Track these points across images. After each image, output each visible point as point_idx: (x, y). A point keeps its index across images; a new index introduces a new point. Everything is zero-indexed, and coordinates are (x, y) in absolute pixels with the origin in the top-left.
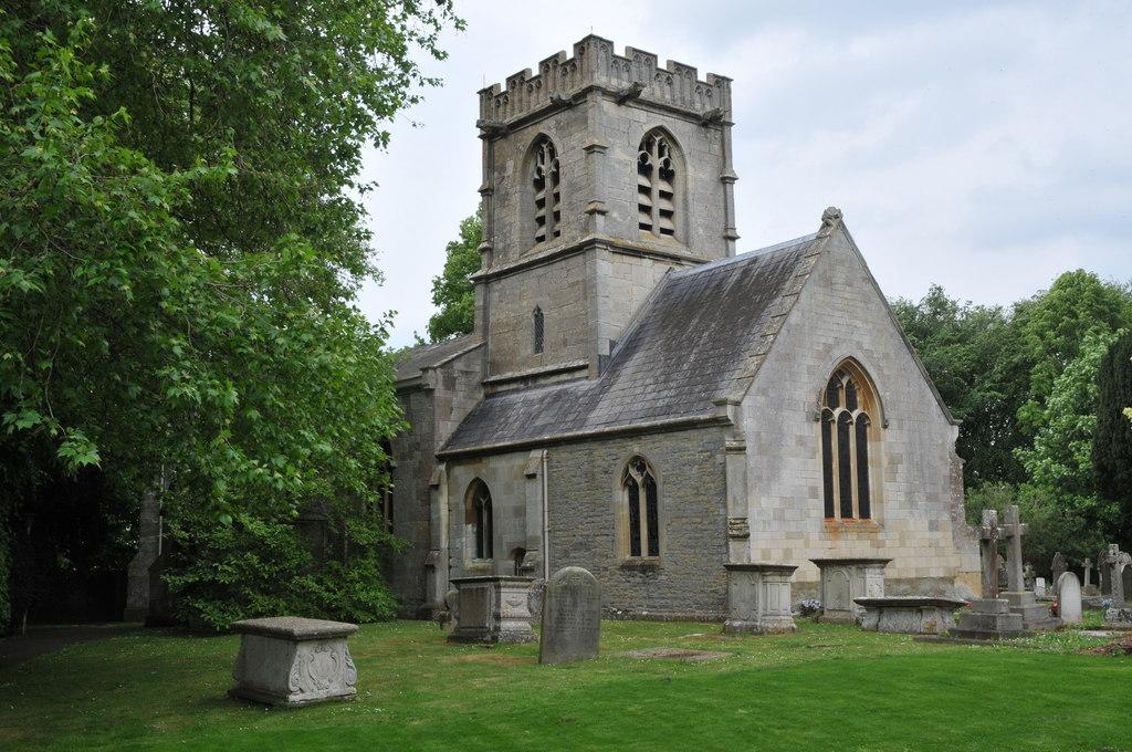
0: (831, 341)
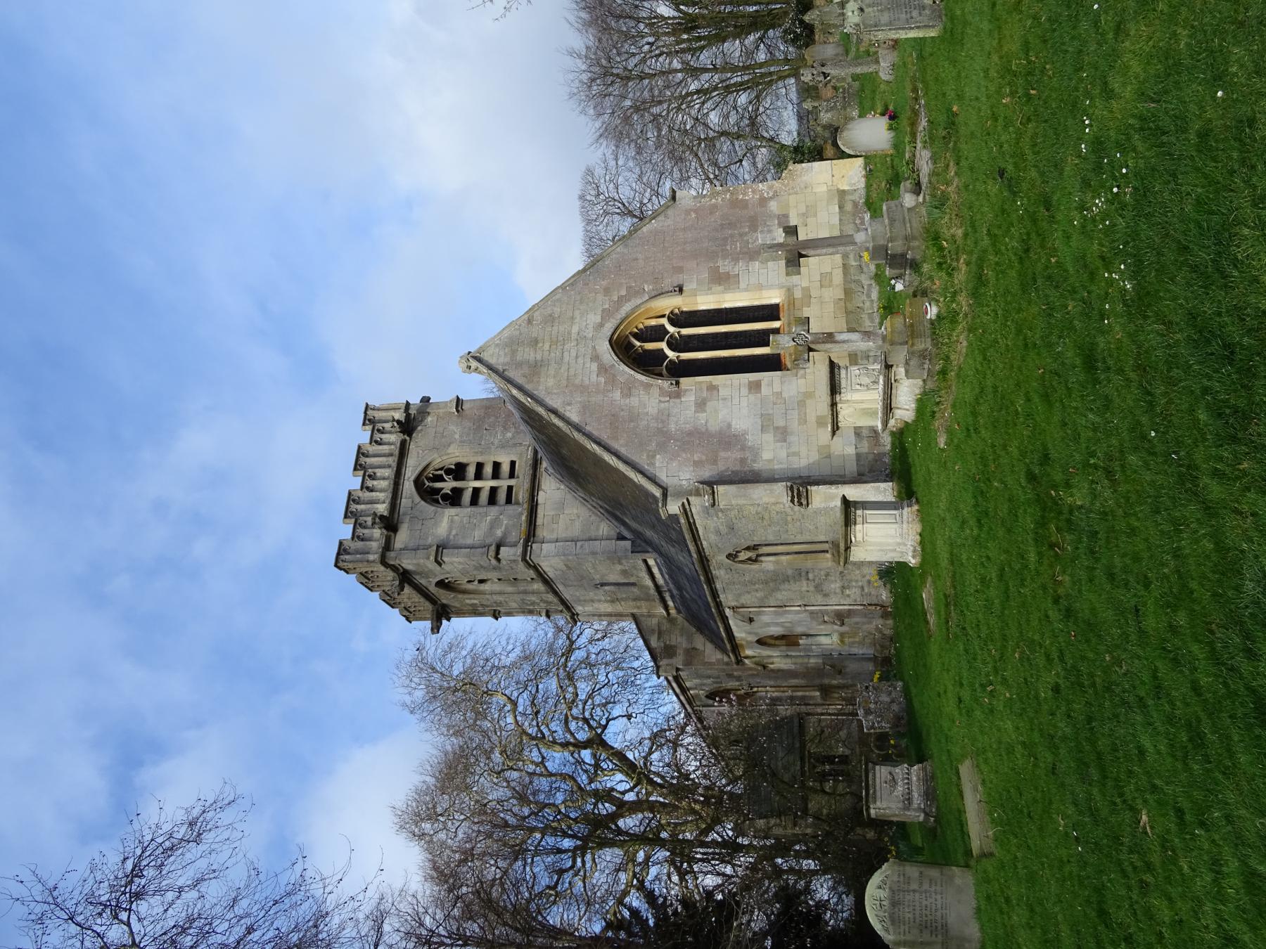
0: (594, 366)
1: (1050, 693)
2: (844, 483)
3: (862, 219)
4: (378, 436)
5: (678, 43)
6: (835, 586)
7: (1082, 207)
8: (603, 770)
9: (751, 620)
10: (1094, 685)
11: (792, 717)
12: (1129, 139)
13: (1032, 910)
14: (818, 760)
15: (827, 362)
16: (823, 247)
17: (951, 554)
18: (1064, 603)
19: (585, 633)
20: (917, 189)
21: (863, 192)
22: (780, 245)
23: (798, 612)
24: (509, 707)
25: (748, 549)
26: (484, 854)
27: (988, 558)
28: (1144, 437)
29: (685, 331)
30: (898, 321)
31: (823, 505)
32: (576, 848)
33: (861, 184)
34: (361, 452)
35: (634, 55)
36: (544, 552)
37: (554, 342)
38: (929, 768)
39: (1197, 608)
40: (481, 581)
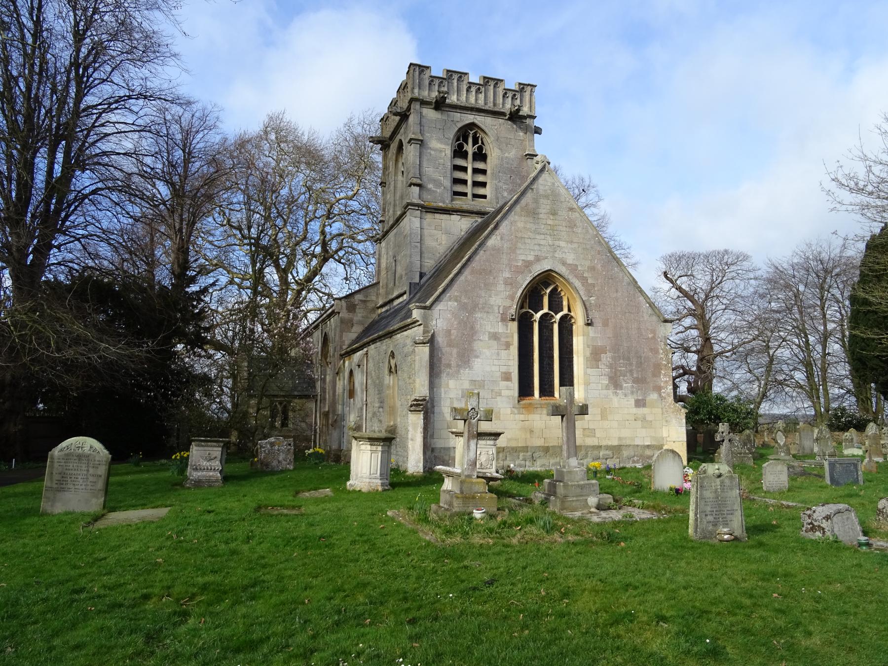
0: (531, 258)
3: (638, 462)
4: (510, 94)
15: (499, 431)
16: (568, 433)
23: (362, 400)
24: (350, 193)
29: (556, 327)
31: (410, 422)
34: (497, 82)
36: (413, 219)
37: (553, 228)
38: (217, 484)
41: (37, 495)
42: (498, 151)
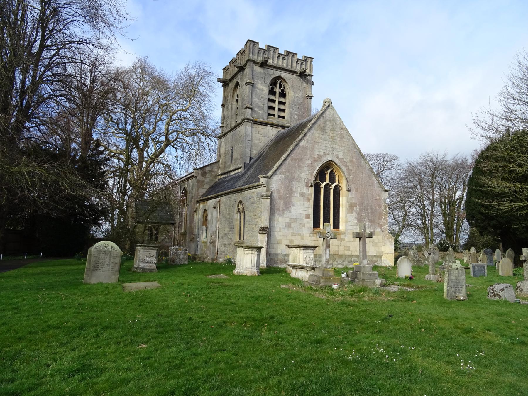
0: (321, 153)
1: (189, 317)
2: (267, 248)
4: (300, 62)
5: (445, 198)
6: (226, 241)
7: (379, 344)
8: (156, 144)
9: (214, 208)
10: (194, 332)
11: (174, 220)
12: (408, 363)
13: (104, 303)
14: (157, 229)
15: (316, 245)
16: (363, 247)
17: (240, 286)
18: (224, 325)
19: (214, 143)
20: (383, 285)
21: (380, 265)
22: (365, 230)
23: (216, 226)
24: (184, 108)
25: (243, 209)
26: (127, 94)
27: (239, 299)
28: (292, 358)
29: (332, 191)
30: (332, 274)
32: (127, 131)
33: (384, 265)
34: (294, 54)
35: (442, 180)
36: (248, 127)
37: (332, 138)
39: (227, 371)
40: (237, 100)
41: (81, 273)
42: (293, 93)
